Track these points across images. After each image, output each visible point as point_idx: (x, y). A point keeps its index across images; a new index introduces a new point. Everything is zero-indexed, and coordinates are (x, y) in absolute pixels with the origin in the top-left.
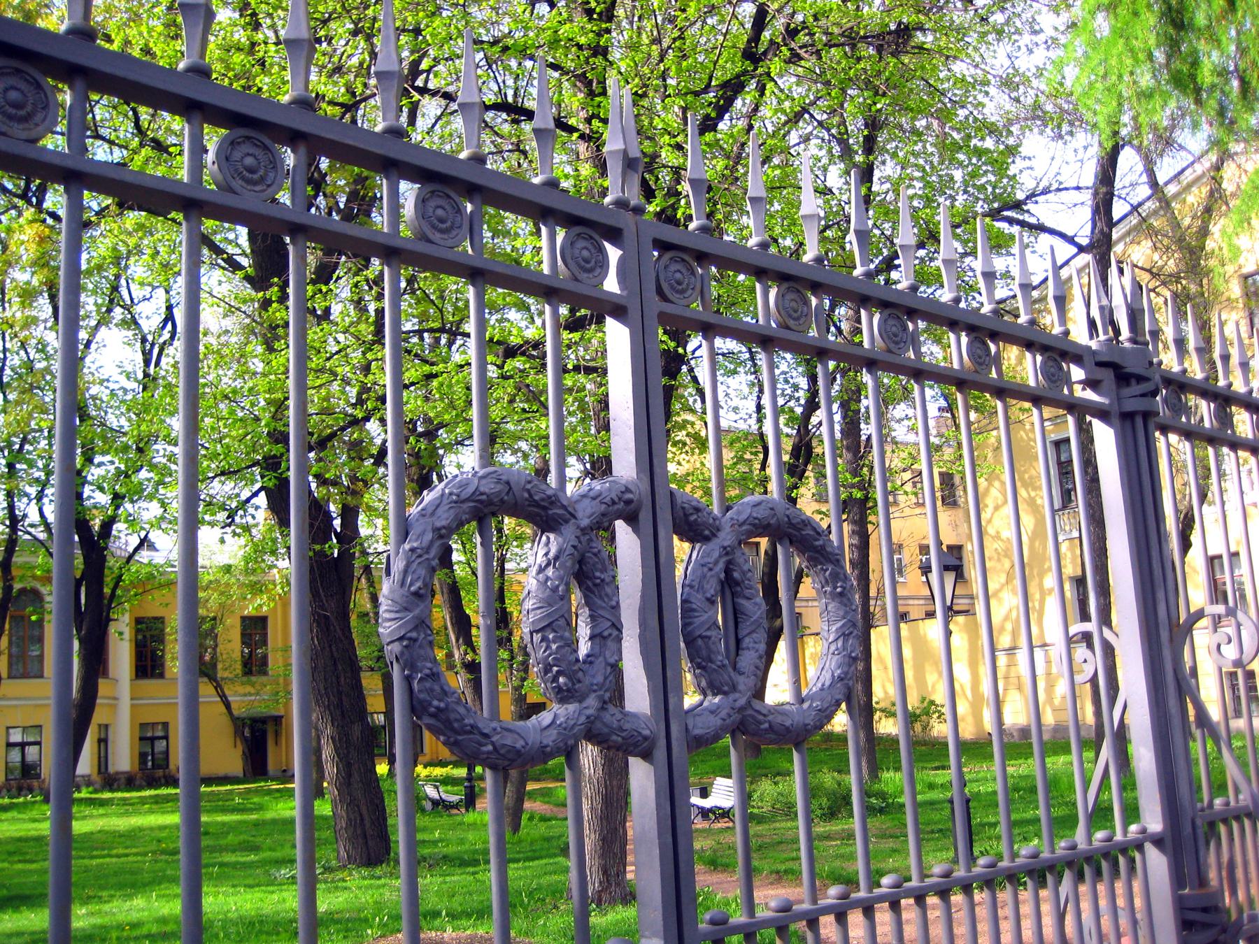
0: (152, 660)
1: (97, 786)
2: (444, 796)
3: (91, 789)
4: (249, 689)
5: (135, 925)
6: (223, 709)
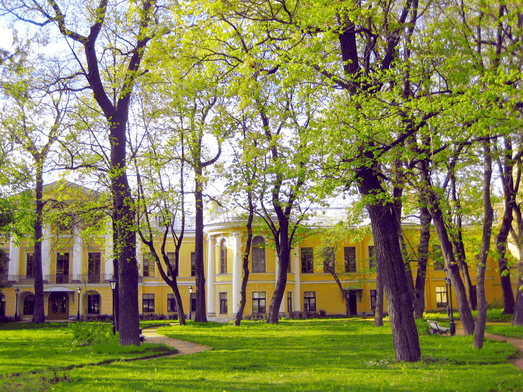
0: (308, 266)
1: (288, 317)
2: (440, 328)
3: (285, 318)
4: (348, 278)
5: (305, 385)
6: (337, 286)
